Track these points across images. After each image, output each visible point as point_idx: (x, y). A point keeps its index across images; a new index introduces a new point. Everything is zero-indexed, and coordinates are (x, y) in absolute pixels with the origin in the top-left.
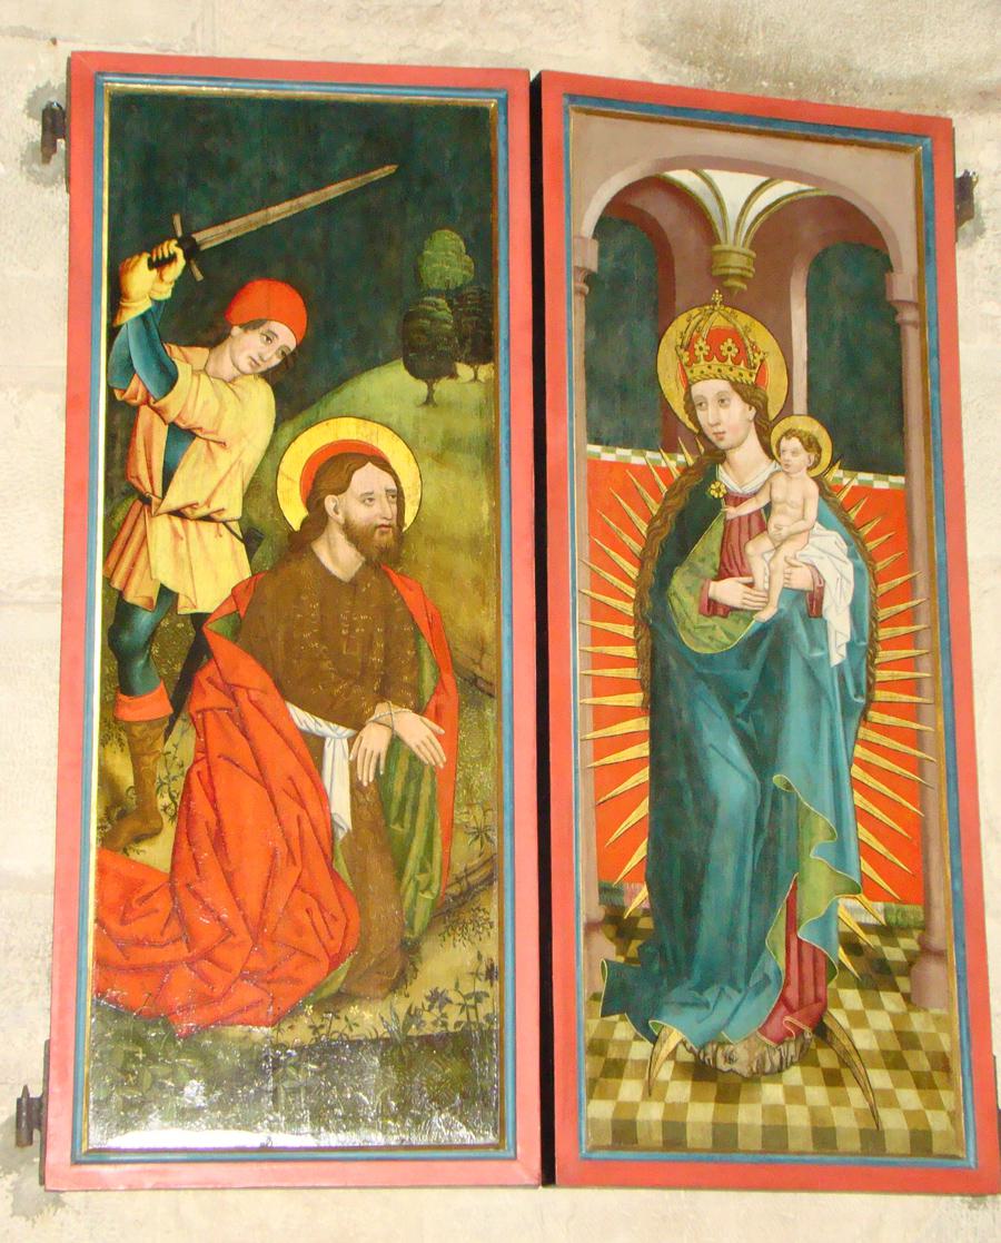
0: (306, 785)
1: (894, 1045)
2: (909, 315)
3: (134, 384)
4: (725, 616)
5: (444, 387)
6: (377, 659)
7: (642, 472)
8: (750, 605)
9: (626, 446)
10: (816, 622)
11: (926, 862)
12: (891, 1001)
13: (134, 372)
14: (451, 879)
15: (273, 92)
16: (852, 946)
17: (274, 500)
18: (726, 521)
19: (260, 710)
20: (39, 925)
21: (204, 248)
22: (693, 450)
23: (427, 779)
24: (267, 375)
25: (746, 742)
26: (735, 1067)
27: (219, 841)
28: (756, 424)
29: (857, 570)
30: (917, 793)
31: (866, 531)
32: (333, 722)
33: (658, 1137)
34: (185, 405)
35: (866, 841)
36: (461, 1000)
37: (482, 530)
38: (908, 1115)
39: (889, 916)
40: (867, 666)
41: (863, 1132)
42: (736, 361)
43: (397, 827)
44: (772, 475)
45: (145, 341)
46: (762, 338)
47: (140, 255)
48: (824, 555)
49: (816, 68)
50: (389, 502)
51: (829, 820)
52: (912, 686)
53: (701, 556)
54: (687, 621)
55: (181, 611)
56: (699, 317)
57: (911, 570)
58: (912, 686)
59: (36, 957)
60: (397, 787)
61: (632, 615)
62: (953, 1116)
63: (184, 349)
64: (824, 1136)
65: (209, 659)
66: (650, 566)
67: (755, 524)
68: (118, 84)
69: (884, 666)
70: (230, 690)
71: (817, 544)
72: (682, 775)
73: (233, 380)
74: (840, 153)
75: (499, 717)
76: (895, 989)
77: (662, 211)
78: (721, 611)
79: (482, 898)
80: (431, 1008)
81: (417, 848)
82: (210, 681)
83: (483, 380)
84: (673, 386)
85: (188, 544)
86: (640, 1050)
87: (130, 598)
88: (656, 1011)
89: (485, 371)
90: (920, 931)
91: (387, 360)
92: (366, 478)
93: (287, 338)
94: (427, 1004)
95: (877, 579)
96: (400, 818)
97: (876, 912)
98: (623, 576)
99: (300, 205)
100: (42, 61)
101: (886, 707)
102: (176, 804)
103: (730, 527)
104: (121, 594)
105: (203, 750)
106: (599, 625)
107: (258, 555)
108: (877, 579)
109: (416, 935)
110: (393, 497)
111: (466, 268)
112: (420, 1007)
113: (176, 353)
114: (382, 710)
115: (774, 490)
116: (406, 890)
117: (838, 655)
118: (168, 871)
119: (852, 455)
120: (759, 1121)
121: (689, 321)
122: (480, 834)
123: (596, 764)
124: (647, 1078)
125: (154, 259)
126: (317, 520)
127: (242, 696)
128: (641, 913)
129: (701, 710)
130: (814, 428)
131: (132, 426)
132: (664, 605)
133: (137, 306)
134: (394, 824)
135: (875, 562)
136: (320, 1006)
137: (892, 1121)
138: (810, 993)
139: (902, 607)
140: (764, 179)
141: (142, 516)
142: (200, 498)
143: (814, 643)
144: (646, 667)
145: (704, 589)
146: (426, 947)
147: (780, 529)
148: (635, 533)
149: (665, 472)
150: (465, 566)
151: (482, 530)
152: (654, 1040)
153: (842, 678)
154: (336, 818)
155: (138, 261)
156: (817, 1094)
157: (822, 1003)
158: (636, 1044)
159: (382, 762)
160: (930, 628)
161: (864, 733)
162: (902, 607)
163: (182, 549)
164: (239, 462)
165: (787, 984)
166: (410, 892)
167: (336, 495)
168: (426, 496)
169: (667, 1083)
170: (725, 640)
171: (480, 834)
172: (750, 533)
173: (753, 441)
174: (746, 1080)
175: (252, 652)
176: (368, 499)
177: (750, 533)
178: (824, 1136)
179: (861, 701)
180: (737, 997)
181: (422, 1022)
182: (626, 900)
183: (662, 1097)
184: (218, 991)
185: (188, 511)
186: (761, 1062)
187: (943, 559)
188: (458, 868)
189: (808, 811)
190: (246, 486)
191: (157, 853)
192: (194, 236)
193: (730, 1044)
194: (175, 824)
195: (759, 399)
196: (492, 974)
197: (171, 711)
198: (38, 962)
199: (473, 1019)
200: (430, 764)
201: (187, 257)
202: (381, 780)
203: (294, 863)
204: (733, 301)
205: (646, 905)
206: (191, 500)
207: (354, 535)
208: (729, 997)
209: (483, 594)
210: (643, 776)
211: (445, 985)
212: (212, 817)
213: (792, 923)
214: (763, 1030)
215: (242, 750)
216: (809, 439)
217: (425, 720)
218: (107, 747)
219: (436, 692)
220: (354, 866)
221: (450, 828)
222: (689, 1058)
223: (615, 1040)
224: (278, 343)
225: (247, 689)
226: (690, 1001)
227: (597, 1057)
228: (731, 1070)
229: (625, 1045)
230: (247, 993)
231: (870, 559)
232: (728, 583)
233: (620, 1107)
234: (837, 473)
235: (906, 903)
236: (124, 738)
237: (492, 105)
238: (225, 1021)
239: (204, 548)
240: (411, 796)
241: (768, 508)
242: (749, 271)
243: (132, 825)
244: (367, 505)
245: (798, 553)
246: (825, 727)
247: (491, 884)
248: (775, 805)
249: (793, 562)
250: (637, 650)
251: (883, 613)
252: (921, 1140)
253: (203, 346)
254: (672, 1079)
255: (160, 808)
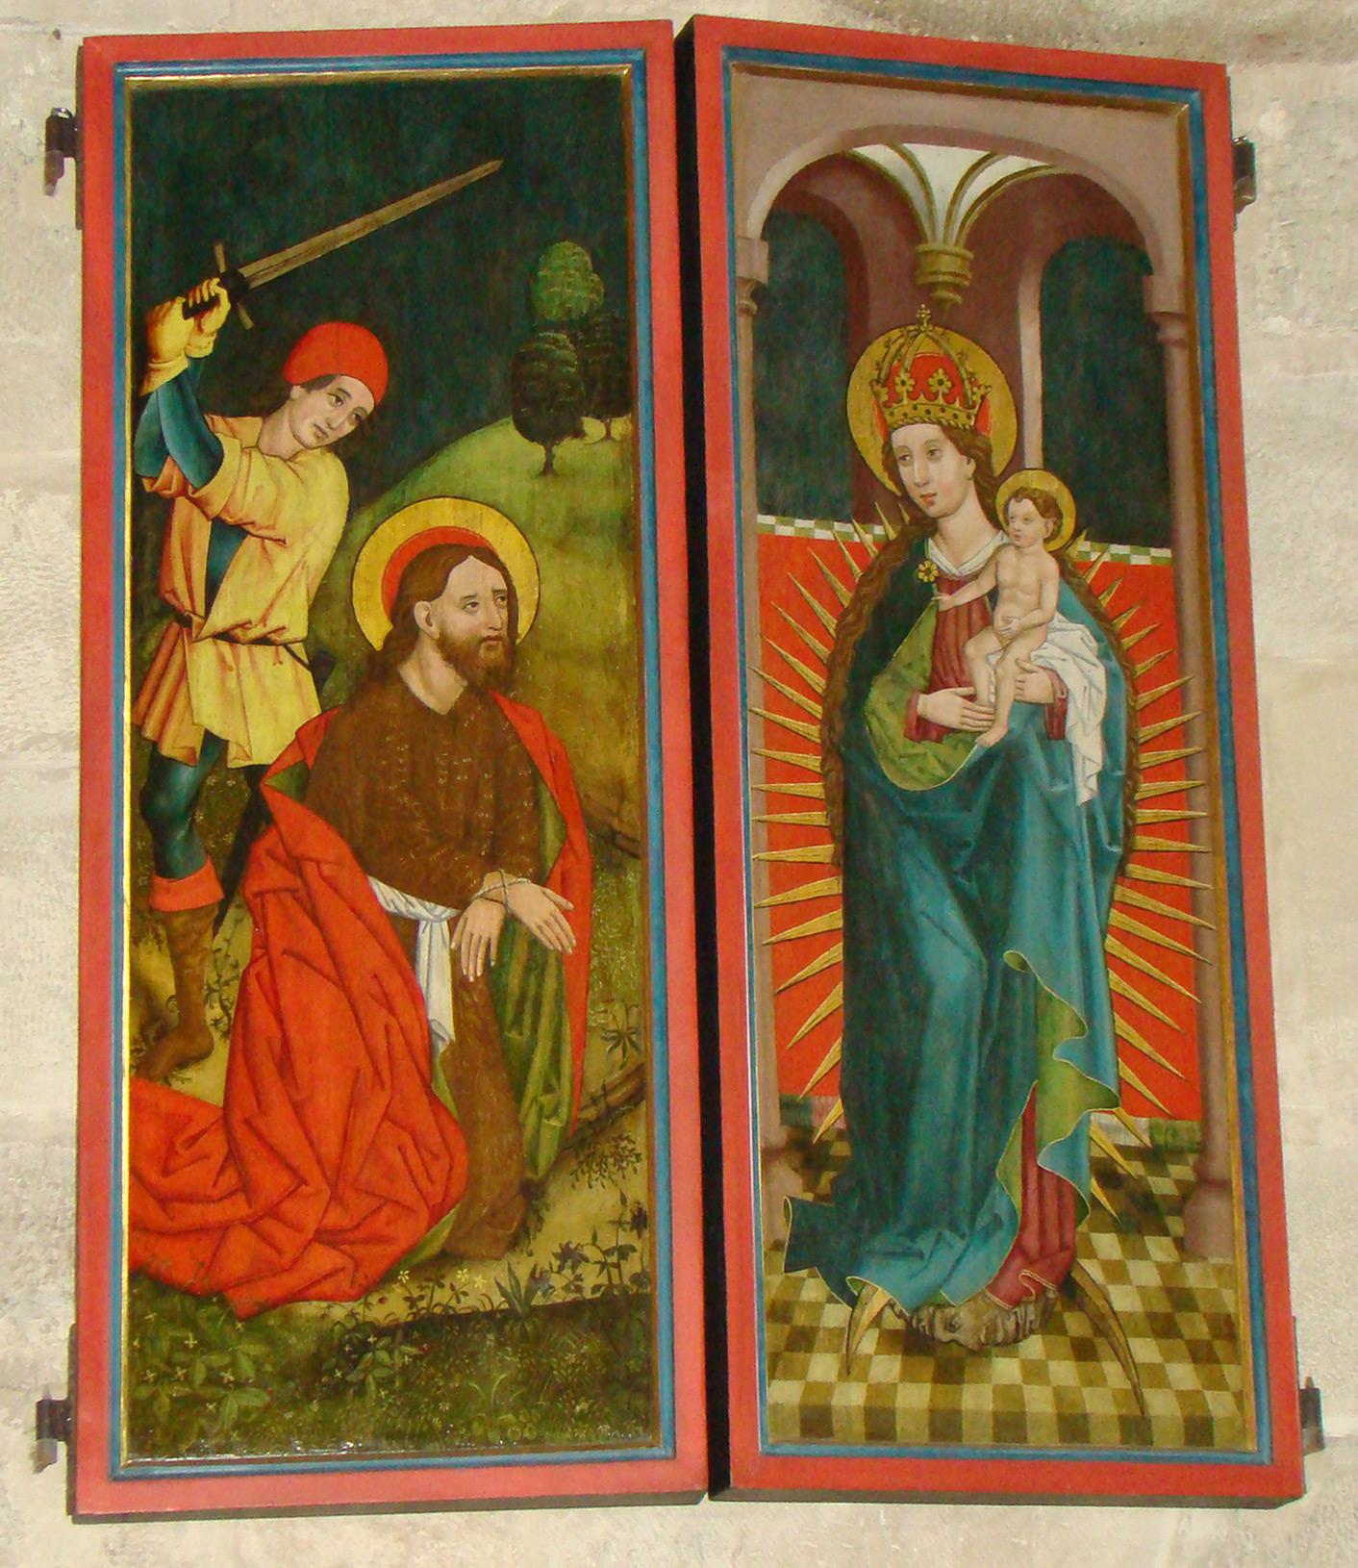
0: (394, 984)
1: (1162, 1306)
2: (1174, 331)
3: (167, 469)
4: (939, 740)
5: (567, 450)
6: (484, 815)
7: (831, 547)
8: (971, 724)
9: (808, 516)
10: (1058, 746)
11: (1205, 1063)
12: (1160, 1249)
13: (168, 454)
14: (585, 1100)
15: (341, 73)
16: (1107, 1175)
17: (349, 610)
18: (938, 614)
19: (336, 890)
20: (57, 1186)
21: (254, 284)
22: (895, 518)
23: (551, 971)
24: (340, 448)
25: (971, 910)
26: (956, 1335)
27: (285, 1064)
28: (977, 483)
29: (1111, 676)
30: (1191, 971)
31: (1121, 622)
32: (429, 901)
33: (859, 1427)
34: (232, 494)
35: (1125, 1036)
36: (600, 1257)
37: (618, 636)
38: (1182, 1395)
39: (1156, 1136)
40: (1125, 805)
41: (1123, 1420)
42: (949, 399)
43: (513, 1035)
44: (998, 549)
45: (180, 412)
46: (983, 367)
47: (173, 300)
48: (1066, 656)
49: (1042, 14)
50: (498, 606)
51: (1077, 1009)
52: (1183, 828)
53: (907, 659)
54: (890, 748)
55: (231, 765)
56: (901, 341)
57: (1180, 674)
58: (1183, 828)
59: (54, 1228)
60: (513, 980)
61: (818, 741)
62: (1239, 1396)
63: (230, 420)
64: (1073, 1426)
65: (268, 824)
66: (841, 675)
67: (976, 616)
68: (138, 78)
69: (1146, 802)
70: (295, 864)
71: (1057, 641)
72: (886, 953)
73: (293, 457)
74: (1080, 116)
75: (644, 881)
76: (1164, 1231)
77: (853, 202)
78: (934, 735)
79: (626, 1122)
80: (561, 1268)
81: (540, 1060)
82: (271, 853)
83: (618, 438)
84: (867, 434)
85: (239, 676)
86: (835, 1315)
87: (166, 750)
88: (855, 1263)
89: (620, 426)
90: (1197, 1155)
91: (494, 418)
92: (468, 577)
93: (361, 396)
94: (556, 1263)
95: (1136, 686)
96: (518, 1021)
97: (1138, 1130)
98: (807, 690)
99: (377, 221)
100: (43, 60)
101: (1151, 858)
102: (228, 1015)
103: (945, 620)
104: (155, 745)
105: (262, 943)
106: (776, 817)
107: (329, 685)
108: (1136, 686)
109: (540, 1174)
110: (503, 599)
111: (594, 290)
112: (548, 1268)
113: (219, 424)
114: (492, 881)
115: (1000, 570)
116: (526, 1116)
117: (1086, 789)
118: (221, 1104)
119: (1100, 523)
120: (989, 1407)
121: (888, 347)
122: (619, 1038)
123: (773, 939)
124: (844, 1351)
125: (191, 304)
126: (404, 635)
127: (310, 869)
128: (834, 1135)
129: (908, 863)
130: (1053, 486)
131: (165, 527)
132: (860, 728)
133: (171, 366)
134: (509, 1031)
135: (1134, 665)
136: (416, 1271)
137: (1161, 1405)
138: (1054, 1239)
139: (1170, 723)
140: (982, 154)
141: (180, 641)
142: (252, 613)
143: (1054, 773)
144: (837, 810)
145: (911, 704)
146: (553, 1190)
147: (1010, 622)
148: (821, 632)
149: (858, 550)
150: (597, 686)
151: (618, 636)
152: (853, 1301)
153: (1092, 820)
154: (434, 1026)
155: (169, 309)
156: (1064, 1371)
157: (1070, 1253)
158: (829, 1307)
159: (493, 949)
160: (1205, 751)
161: (1122, 893)
162: (1170, 723)
163: (232, 683)
164: (303, 564)
165: (1024, 1227)
166: (531, 1121)
167: (429, 601)
168: (547, 592)
169: (869, 1358)
170: (940, 772)
171: (619, 1038)
172: (970, 625)
173: (972, 507)
174: (972, 1352)
175: (322, 812)
176: (470, 603)
177: (970, 625)
178: (1073, 1426)
179: (1117, 850)
180: (959, 1245)
181: (551, 1287)
182: (815, 1119)
183: (863, 1377)
184: (290, 1253)
185: (239, 632)
186: (992, 1330)
187: (1224, 657)
188: (594, 1087)
189: (1050, 998)
190: (312, 596)
191: (206, 1081)
192: (241, 270)
193: (950, 1306)
194: (228, 1042)
195: (979, 448)
196: (640, 1221)
197: (220, 894)
198: (56, 1234)
199: (616, 1281)
200: (556, 950)
201: (232, 298)
202: (493, 974)
203: (382, 1085)
204: (945, 319)
205: (841, 1125)
206: (241, 618)
207: (454, 654)
208: (951, 1246)
209: (622, 721)
210: (835, 953)
211: (580, 1238)
212: (275, 1031)
213: (1030, 1147)
214: (993, 1288)
215: (312, 942)
216: (1045, 502)
217: (549, 891)
218: (141, 945)
219: (562, 854)
220: (458, 1084)
221: (582, 1034)
222: (899, 1324)
223: (804, 1303)
224: (351, 405)
225: (318, 862)
226: (899, 1250)
227: (779, 1325)
228: (953, 1341)
229: (816, 1308)
230: (322, 1259)
231: (1127, 659)
232: (942, 696)
233: (810, 1388)
234: (1083, 545)
235: (1176, 1118)
236: (162, 932)
237: (625, 72)
238: (301, 1295)
239: (259, 679)
240: (531, 992)
241: (994, 595)
242: (965, 277)
243: (173, 1047)
244: (470, 612)
245: (1033, 654)
246: (1070, 891)
247: (637, 1104)
248: (1007, 990)
249: (1027, 666)
250: (825, 787)
251: (1146, 732)
252: (1199, 1430)
253: (254, 415)
254: (877, 1353)
255: (209, 1022)
